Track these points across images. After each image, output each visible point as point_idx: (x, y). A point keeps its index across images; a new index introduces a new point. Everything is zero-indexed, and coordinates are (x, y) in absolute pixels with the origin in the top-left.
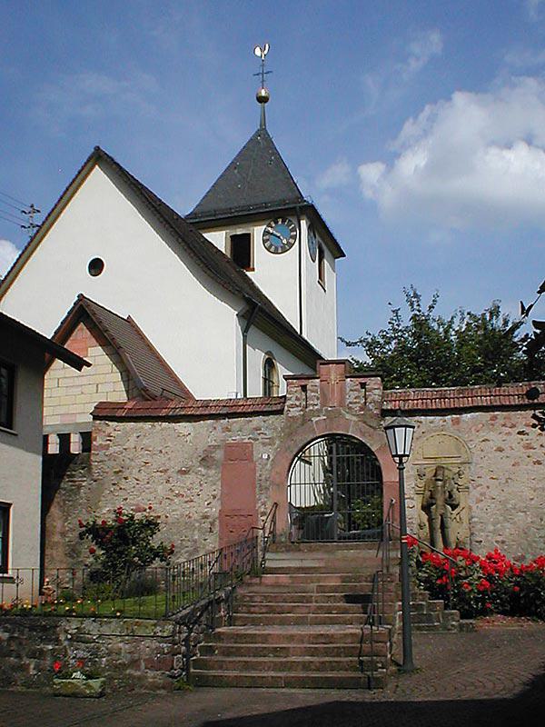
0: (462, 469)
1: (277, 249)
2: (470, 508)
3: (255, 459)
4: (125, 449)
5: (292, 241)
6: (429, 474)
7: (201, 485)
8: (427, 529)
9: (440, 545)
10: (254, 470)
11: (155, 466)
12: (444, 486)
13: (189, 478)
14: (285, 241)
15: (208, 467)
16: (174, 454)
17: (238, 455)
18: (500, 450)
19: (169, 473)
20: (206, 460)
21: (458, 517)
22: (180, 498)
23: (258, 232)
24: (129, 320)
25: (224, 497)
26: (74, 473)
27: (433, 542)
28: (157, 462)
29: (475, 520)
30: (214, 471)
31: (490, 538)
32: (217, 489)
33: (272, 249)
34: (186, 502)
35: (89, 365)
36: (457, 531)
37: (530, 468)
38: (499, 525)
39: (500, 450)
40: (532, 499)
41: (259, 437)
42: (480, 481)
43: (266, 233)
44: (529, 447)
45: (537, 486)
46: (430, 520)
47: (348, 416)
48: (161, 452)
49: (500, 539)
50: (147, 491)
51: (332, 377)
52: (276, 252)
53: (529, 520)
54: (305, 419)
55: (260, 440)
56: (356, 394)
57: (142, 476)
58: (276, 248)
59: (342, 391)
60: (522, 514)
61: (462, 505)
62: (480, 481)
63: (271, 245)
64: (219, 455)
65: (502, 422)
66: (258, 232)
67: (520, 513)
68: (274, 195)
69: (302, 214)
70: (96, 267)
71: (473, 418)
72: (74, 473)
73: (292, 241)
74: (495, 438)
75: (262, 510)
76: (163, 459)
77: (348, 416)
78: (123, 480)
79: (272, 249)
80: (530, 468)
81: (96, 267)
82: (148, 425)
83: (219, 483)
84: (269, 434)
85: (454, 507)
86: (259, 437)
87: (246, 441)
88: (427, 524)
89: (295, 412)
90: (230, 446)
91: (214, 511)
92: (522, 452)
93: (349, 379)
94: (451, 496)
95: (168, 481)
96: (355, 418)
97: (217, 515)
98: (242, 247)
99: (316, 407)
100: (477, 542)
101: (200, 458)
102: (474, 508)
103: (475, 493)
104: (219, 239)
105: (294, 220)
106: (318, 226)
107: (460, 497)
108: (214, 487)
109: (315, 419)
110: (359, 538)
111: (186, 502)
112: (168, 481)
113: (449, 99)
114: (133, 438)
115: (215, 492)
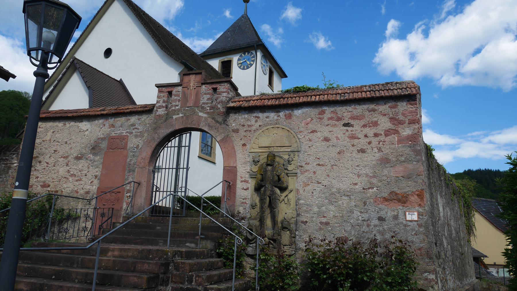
0: (292, 156)
1: (244, 66)
2: (298, 190)
3: (128, 148)
4: (43, 141)
5: (252, 63)
6: (263, 159)
7: (88, 168)
8: (258, 209)
9: (269, 222)
10: (126, 157)
11: (61, 153)
12: (273, 171)
13: (83, 164)
14: (248, 63)
15: (95, 154)
16: (75, 145)
17: (116, 145)
18: (327, 140)
19: (70, 158)
20: (95, 149)
21: (286, 200)
22: (73, 178)
23: (235, 59)
24: (121, 83)
25: (101, 179)
26: (7, 158)
27: (262, 220)
28: (63, 150)
29: (302, 202)
30: (98, 157)
31: (314, 219)
32: (97, 171)
33: (246, 68)
34: (77, 181)
35: (14, 77)
36: (285, 211)
37: (354, 155)
38: (324, 208)
39: (327, 140)
40: (356, 184)
41: (134, 131)
42: (307, 167)
43: (239, 60)
44: (353, 137)
45: (361, 172)
46: (262, 201)
47: (201, 114)
48: (66, 143)
49: (324, 220)
50: (53, 172)
51: (192, 84)
52: (244, 69)
53: (353, 204)
54: (168, 116)
55: (134, 134)
56: (209, 96)
57: (51, 161)
58: (244, 67)
59: (197, 95)
60: (346, 198)
61: (290, 188)
62: (307, 167)
63: (244, 67)
64: (104, 145)
65: (329, 116)
66: (235, 59)
67: (344, 197)
68: (242, 41)
69: (258, 49)
70: (108, 53)
71: (185, 36)
72: (7, 158)
73: (252, 63)
74: (324, 131)
75: (128, 188)
76: (67, 148)
77: (201, 114)
78: (38, 163)
79: (246, 68)
80: (354, 155)
81: (108, 53)
82: (60, 124)
83: (101, 166)
84: (141, 128)
85: (283, 189)
86: (134, 131)
87: (124, 134)
88: (258, 204)
89: (161, 112)
90: (113, 138)
91: (94, 188)
92: (346, 142)
93: (204, 86)
94: (279, 179)
95: (67, 165)
96: (205, 115)
97: (95, 191)
98: (227, 66)
99: (177, 108)
100: (302, 222)
101: (91, 148)
102: (301, 191)
103: (302, 178)
104: (215, 64)
105: (254, 52)
106: (268, 56)
107: (292, 183)
108: (97, 169)
109: (174, 117)
110: (163, 213)
111: (77, 181)
112: (67, 165)
113: (376, 56)
114: (50, 134)
115: (97, 174)
